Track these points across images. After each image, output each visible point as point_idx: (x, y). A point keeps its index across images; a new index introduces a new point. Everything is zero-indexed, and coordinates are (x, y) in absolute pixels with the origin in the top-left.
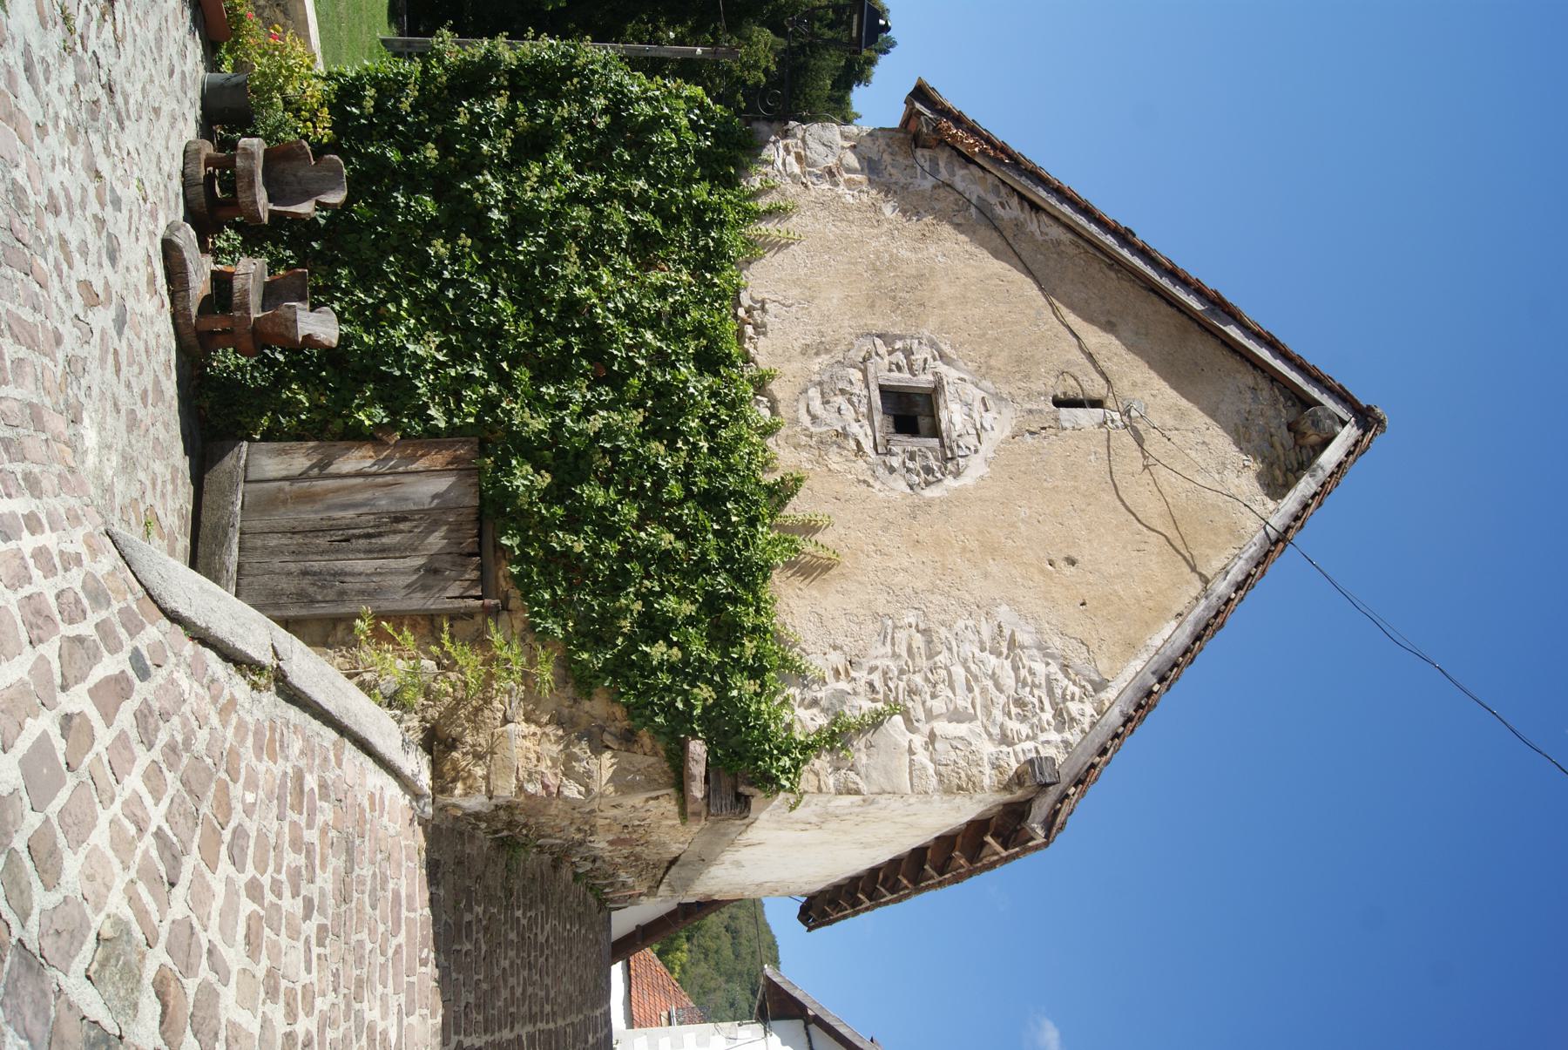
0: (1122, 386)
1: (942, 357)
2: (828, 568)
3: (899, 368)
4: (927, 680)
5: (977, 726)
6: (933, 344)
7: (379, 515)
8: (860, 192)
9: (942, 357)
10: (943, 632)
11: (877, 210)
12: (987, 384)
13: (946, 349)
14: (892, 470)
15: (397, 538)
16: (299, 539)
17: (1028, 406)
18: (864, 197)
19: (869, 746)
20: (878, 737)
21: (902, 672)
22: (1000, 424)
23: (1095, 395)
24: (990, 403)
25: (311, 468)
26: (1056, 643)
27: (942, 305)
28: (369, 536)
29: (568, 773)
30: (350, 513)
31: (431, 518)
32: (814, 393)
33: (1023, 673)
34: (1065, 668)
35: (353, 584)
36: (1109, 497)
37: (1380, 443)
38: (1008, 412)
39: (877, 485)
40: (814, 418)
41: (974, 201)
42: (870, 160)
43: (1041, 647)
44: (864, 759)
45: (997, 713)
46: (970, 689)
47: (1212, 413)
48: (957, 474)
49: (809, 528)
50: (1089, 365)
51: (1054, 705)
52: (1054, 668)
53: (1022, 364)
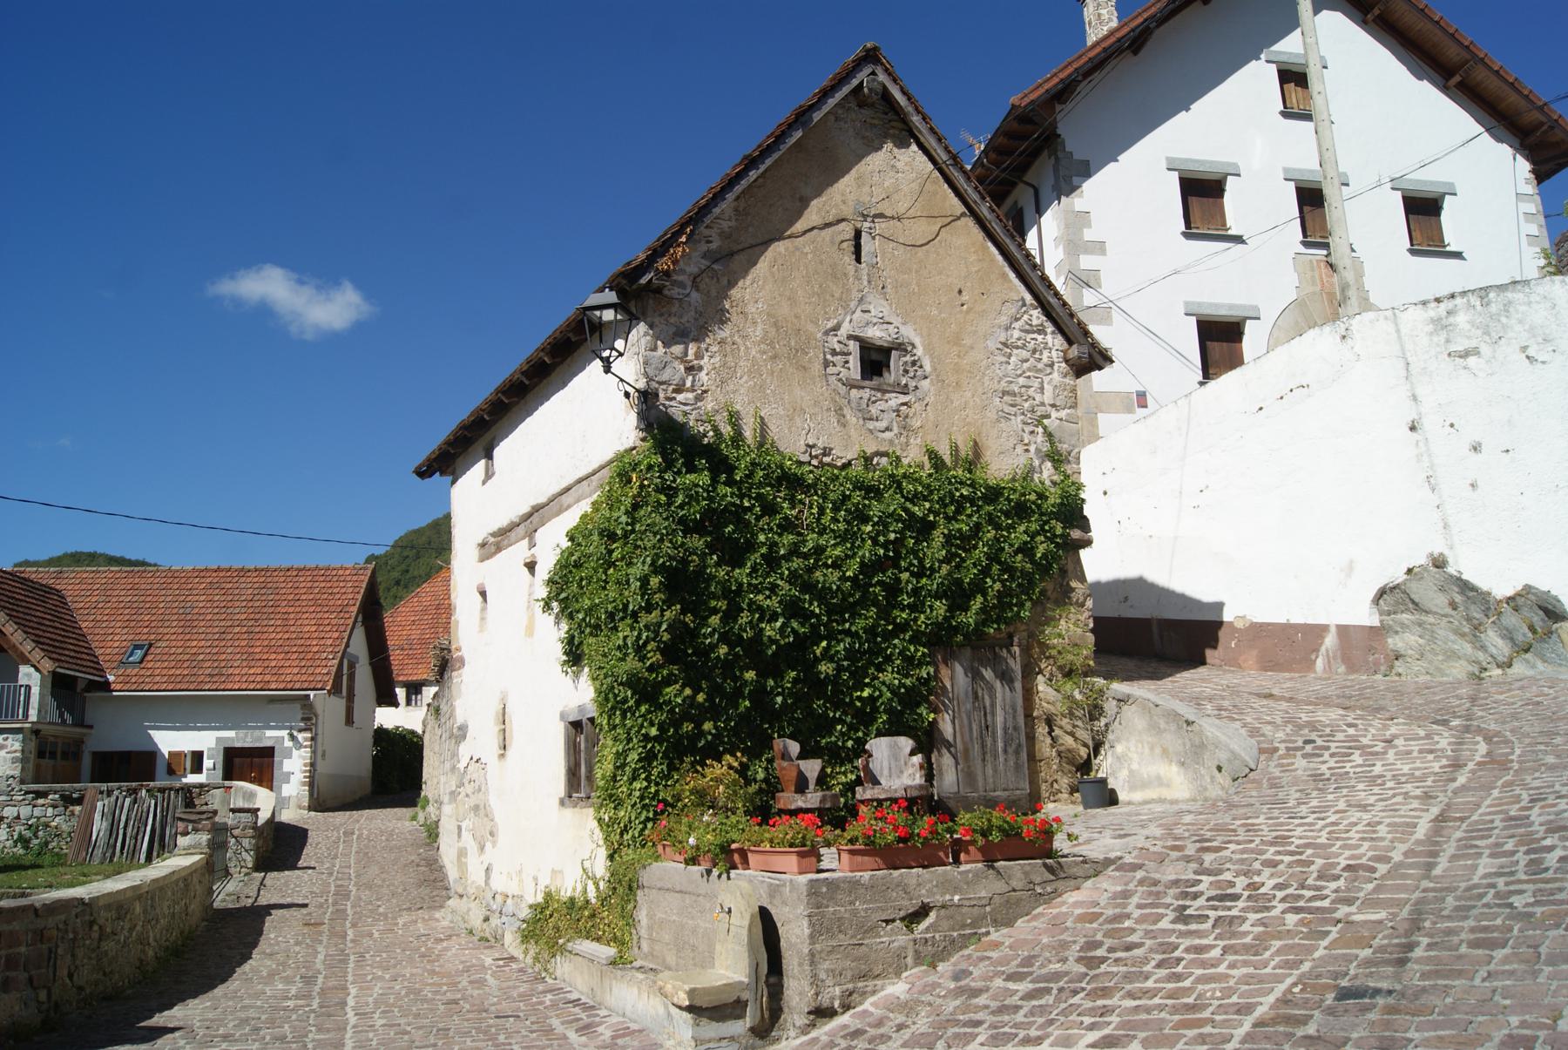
0: (847, 211)
1: (836, 328)
2: (975, 442)
3: (847, 362)
4: (1026, 400)
5: (1046, 379)
6: (826, 333)
7: (974, 708)
8: (707, 350)
9: (836, 328)
10: (1003, 384)
11: (722, 342)
12: (853, 304)
13: (830, 325)
14: (916, 387)
15: (986, 697)
16: (988, 757)
17: (865, 283)
18: (714, 348)
19: (1060, 442)
20: (1057, 435)
21: (1023, 414)
22: (878, 307)
23: (850, 234)
24: (865, 307)
25: (950, 752)
26: (1004, 320)
27: (797, 317)
28: (985, 714)
29: (1082, 605)
30: (975, 727)
31: (976, 676)
32: (871, 425)
33: (1019, 343)
34: (1017, 320)
35: (1010, 724)
36: (921, 252)
37: (886, 53)
38: (870, 298)
39: (927, 399)
40: (888, 429)
41: (708, 263)
42: (675, 334)
43: (1008, 328)
44: (1065, 446)
45: (1040, 366)
46: (1029, 377)
47: (860, 158)
48: (914, 346)
49: (955, 450)
50: (833, 228)
51: (1034, 332)
52: (1017, 325)
53: (836, 275)
